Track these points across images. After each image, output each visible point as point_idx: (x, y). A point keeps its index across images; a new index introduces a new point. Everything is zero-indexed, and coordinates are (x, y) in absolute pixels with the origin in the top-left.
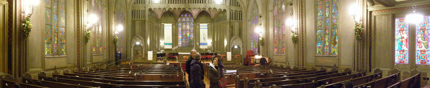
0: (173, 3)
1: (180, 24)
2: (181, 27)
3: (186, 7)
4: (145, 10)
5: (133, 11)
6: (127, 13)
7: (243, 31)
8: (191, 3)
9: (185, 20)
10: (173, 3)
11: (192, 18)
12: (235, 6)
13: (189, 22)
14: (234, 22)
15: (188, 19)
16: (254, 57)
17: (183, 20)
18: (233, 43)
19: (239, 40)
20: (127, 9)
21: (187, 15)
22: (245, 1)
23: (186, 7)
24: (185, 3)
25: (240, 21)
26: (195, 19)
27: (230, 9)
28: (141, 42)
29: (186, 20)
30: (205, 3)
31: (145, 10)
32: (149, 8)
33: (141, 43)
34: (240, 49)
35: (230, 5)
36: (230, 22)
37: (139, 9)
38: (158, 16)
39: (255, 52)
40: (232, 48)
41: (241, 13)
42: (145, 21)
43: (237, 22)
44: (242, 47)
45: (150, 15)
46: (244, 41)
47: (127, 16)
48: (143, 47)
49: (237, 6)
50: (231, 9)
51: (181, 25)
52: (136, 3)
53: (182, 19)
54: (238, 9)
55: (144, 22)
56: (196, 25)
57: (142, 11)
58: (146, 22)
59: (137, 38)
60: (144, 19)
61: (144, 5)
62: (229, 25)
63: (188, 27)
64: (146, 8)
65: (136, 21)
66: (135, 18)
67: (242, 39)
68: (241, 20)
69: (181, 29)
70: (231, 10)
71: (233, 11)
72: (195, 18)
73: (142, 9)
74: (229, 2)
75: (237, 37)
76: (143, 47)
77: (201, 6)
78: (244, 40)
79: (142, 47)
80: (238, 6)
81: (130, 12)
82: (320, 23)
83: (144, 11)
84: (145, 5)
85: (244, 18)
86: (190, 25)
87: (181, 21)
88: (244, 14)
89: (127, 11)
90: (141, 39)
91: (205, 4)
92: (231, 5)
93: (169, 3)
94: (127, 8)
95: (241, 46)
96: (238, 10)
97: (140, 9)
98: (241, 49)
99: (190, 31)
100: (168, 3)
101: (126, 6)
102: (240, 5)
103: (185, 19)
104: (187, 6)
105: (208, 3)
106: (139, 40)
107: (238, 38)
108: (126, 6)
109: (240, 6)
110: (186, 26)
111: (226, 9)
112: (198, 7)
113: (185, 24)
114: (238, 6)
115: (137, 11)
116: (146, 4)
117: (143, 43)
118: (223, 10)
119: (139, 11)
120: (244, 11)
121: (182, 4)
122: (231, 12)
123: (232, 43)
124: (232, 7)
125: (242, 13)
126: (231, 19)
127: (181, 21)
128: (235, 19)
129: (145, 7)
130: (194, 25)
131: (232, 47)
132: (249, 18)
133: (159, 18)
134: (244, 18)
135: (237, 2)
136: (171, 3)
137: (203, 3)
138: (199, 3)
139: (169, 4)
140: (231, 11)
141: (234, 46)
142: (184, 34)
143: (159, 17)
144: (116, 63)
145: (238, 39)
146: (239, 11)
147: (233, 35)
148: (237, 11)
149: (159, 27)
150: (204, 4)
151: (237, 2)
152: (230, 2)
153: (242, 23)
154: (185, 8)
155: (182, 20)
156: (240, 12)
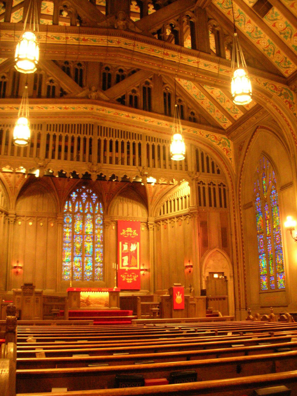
1: (68, 219)
3: (93, 171)
8: (105, 162)
10: (59, 158)
12: (208, 172)
17: (66, 207)
22: (232, 160)
23: (93, 171)
29: (84, 209)
41: (224, 190)
49: (213, 172)
51: (71, 221)
53: (75, 206)
54: (216, 180)
63: (89, 227)
68: (225, 206)
70: (199, 182)
71: (204, 186)
80: (216, 171)
82: (292, 109)
86: (93, 222)
87: (71, 210)
91: (141, 168)
93: (47, 156)
95: (228, 273)
99: (93, 238)
100: (44, 155)
103: (81, 205)
104: (95, 169)
109: (221, 173)
114: (216, 171)
121: (81, 163)
123: (206, 265)
125: (226, 188)
127: (71, 210)
135: (213, 163)
136: (53, 157)
137: (134, 164)
138: (120, 165)
139: (46, 160)
142: (78, 246)
148: (214, 185)
150: (137, 168)
151: (213, 163)
156: (222, 186)
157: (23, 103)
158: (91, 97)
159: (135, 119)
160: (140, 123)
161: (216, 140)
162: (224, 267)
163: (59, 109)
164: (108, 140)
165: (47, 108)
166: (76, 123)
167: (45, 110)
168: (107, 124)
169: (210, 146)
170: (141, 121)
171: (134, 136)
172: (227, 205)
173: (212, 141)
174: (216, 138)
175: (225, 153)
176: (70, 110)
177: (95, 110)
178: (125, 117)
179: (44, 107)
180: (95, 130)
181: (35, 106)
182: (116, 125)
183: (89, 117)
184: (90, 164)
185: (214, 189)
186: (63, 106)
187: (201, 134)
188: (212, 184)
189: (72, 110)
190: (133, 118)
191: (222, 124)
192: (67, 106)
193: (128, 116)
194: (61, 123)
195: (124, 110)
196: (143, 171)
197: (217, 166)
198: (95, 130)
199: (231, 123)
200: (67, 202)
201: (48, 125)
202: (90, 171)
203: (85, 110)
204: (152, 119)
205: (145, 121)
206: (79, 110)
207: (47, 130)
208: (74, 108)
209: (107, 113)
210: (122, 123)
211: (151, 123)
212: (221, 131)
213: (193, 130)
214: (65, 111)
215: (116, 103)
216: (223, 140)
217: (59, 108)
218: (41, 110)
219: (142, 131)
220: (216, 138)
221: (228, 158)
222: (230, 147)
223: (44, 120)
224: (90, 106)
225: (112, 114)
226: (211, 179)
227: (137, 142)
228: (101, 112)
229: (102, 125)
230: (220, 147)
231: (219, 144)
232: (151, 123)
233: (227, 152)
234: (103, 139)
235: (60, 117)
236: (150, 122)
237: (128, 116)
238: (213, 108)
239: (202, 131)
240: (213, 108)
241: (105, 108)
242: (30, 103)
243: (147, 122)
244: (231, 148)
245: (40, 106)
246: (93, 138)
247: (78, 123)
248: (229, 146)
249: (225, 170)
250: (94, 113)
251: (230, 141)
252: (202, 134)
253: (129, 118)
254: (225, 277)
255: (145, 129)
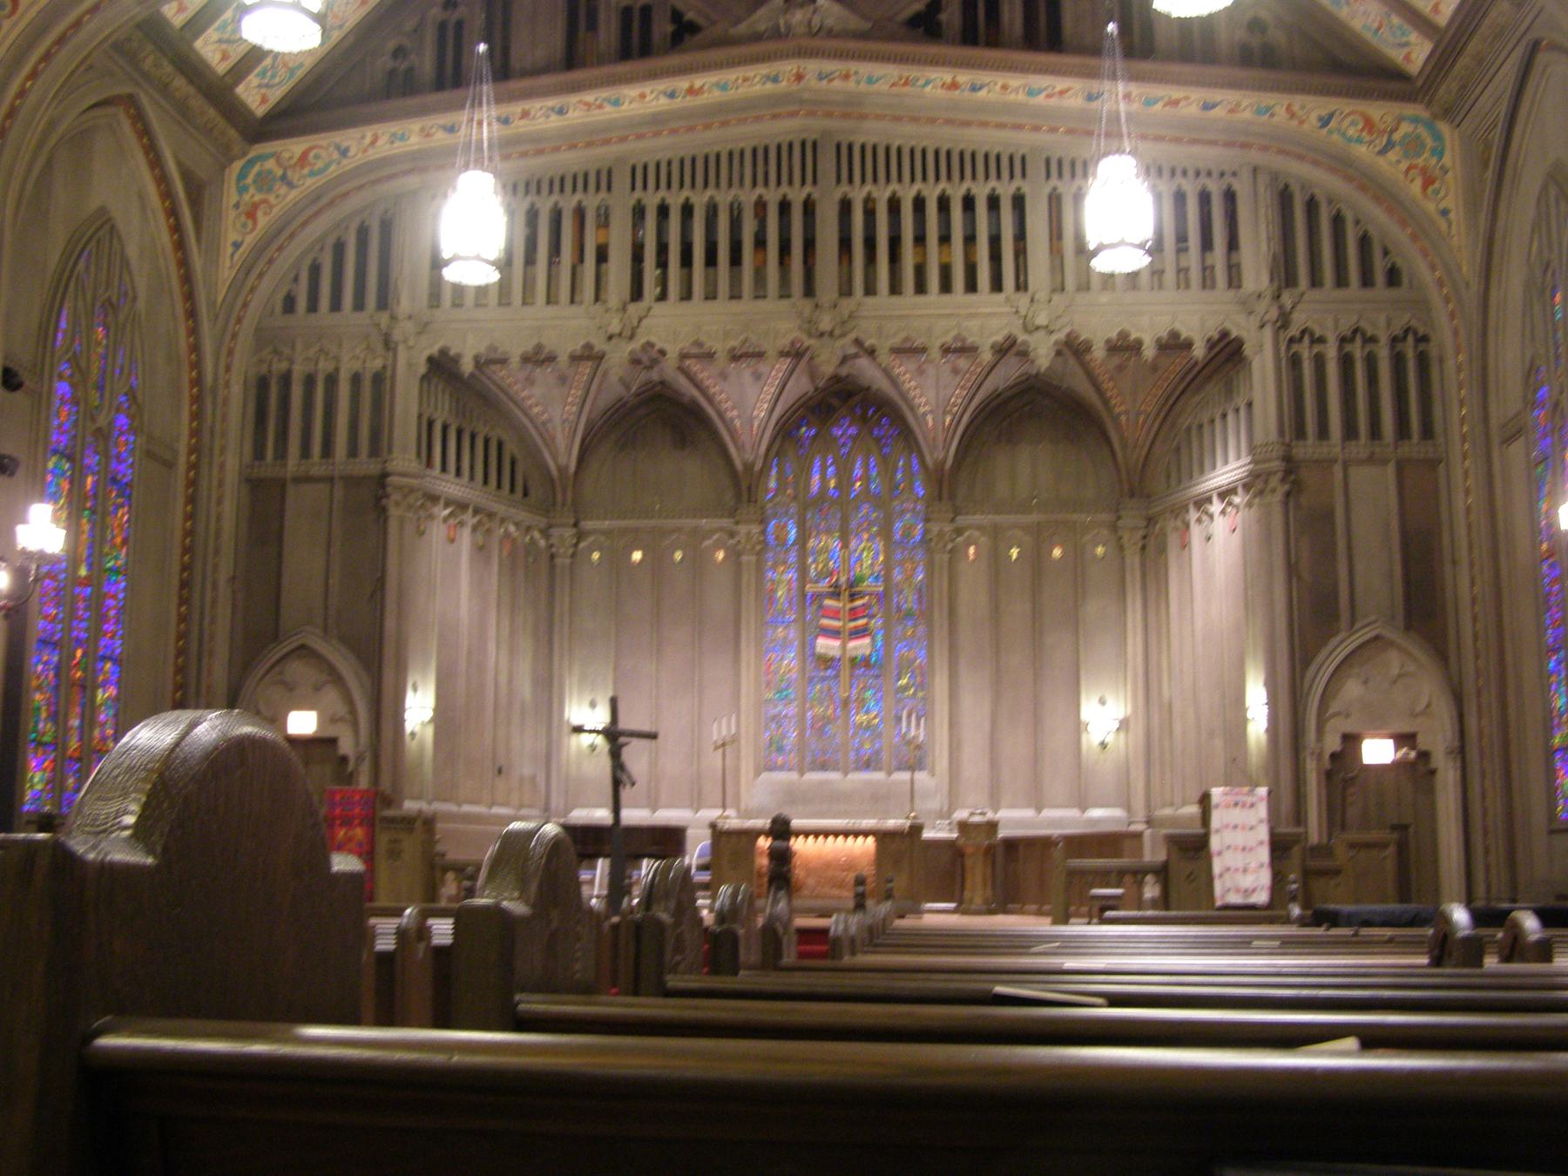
0: (687, 295)
2: (792, 557)
4: (389, 373)
5: (263, 384)
6: (197, 400)
7: (1454, 563)
8: (870, 290)
9: (838, 474)
11: (915, 462)
13: (877, 501)
14: (1338, 470)
15: (865, 473)
16: (488, 102)
17: (816, 479)
18: (1335, 707)
19: (1411, 668)
20: (197, 365)
21: (853, 431)
22: (1452, 216)
24: (809, 291)
25: (1414, 447)
26: (940, 466)
27: (1284, 321)
28: (341, 709)
29: (845, 482)
30: (1026, 289)
31: (384, 367)
32: (434, 350)
33: (334, 720)
34: (1433, 772)
35: (1284, 274)
36: (1288, 472)
37: (325, 366)
38: (550, 442)
39: (79, 518)
40: (1326, 764)
41: (1423, 361)
42: (383, 486)
43: (1371, 459)
44: (1449, 752)
45: (445, 428)
46: (1469, 688)
47: (195, 433)
48: (360, 759)
49: (1367, 280)
50: (1299, 320)
51: (793, 534)
52: (302, 303)
55: (379, 499)
56: (959, 531)
57: (356, 379)
58: (395, 497)
59: (298, 670)
60: (373, 468)
61: (384, 318)
62: (1286, 504)
64: (401, 348)
65: (291, 491)
66: (281, 454)
67: (1453, 660)
68: (1427, 432)
69: (792, 575)
70: (1294, 331)
71: (1317, 349)
72: (940, 455)
73: (357, 366)
74: (1264, 247)
75: (1388, 633)
76: (351, 767)
77: (974, 324)
78: (1469, 667)
79: (344, 760)
80: (1380, 277)
81: (236, 389)
83: (378, 379)
84: (393, 318)
85: (1462, 403)
86: (886, 532)
88: (1450, 365)
89: (197, 382)
90: (337, 679)
92: (1290, 280)
93: (637, 293)
94: (195, 348)
95: (1438, 738)
96: (1381, 325)
97: (337, 359)
98: (1439, 777)
100: (544, 299)
101: (194, 331)
102: (1400, 262)
105: (1054, 291)
106: (317, 689)
107: (1391, 644)
108: (194, 331)
109: (1405, 280)
110: (845, 545)
111: (1241, 327)
112: (943, 334)
113: (836, 523)
114: (1380, 277)
115: (310, 381)
116: (404, 305)
117: (355, 724)
118: (1211, 344)
119: (332, 380)
120: (1456, 333)
121: (771, 305)
122: (1295, 362)
124: (1315, 294)
126: (1300, 433)
128: (1350, 432)
129: (388, 344)
130: (926, 532)
131: (1334, 756)
132: (1508, 398)
133: (562, 470)
134: (1456, 413)
137: (997, 285)
138: (909, 297)
139: (633, 309)
140: (1292, 340)
141: (1352, 741)
143: (563, 452)
144: (472, 897)
145: (1394, 662)
146: (1394, 340)
147: (1335, 616)
149: (558, 561)
150: (1008, 299)
151: (1365, 242)
152: (1277, 247)
153: (1432, 464)
154: (808, 342)
155: (807, 486)
157: (473, 106)
158: (789, 27)
159: (982, 94)
160: (1009, 108)
161: (1370, 132)
162: (1419, 708)
163: (663, 101)
164: (882, 195)
165: (617, 103)
166: (747, 146)
167: (609, 112)
168: (871, 132)
169: (1341, 164)
170: (1012, 97)
171: (994, 164)
172: (1438, 427)
173: (1350, 140)
174: (1369, 125)
175: (1416, 187)
176: (713, 96)
177: (811, 81)
178: (940, 93)
179: (608, 100)
180: (827, 164)
181: (573, 99)
182: (909, 128)
183: (793, 115)
184: (806, 306)
185: (1319, 361)
186: (682, 84)
187: (1292, 115)
188: (1358, 336)
189: (716, 96)
190: (975, 88)
191: (1396, 55)
192: (699, 81)
193: (954, 86)
194: (687, 154)
195: (936, 62)
196: (1032, 309)
197: (1386, 253)
198: (827, 164)
199: (1427, 47)
200: (817, 463)
201: (838, 146)
202: (810, 335)
203: (769, 86)
204: (1060, 83)
205: (1031, 93)
206: (743, 91)
207: (633, 188)
208: (724, 87)
209: (863, 87)
210: (932, 121)
211: (1053, 102)
212: (1394, 86)
213: (1251, 105)
214: (691, 102)
215: (901, 40)
216: (1405, 128)
217: (665, 93)
218: (597, 111)
219: (1023, 141)
220: (1369, 125)
221: (1431, 207)
222: (1441, 156)
223: (615, 149)
224: (788, 67)
225: (883, 87)
226: (1355, 318)
227: (1006, 190)
228: (837, 84)
229: (851, 138)
230: (1391, 166)
231: (1383, 152)
232: (1053, 102)
233: (1428, 182)
234: (858, 195)
235: (674, 132)
236: (1049, 96)
237: (954, 86)
238: (277, 80)
239: (1298, 101)
240: (277, 80)
241: (853, 66)
242: (499, 100)
243: (1040, 99)
244: (1447, 160)
245: (590, 97)
246: (816, 196)
247: (669, 155)
248: (1438, 152)
249: (1421, 266)
250: (806, 96)
251: (1444, 128)
252: (1300, 113)
253: (957, 92)
254: (1424, 756)
255: (1036, 129)
